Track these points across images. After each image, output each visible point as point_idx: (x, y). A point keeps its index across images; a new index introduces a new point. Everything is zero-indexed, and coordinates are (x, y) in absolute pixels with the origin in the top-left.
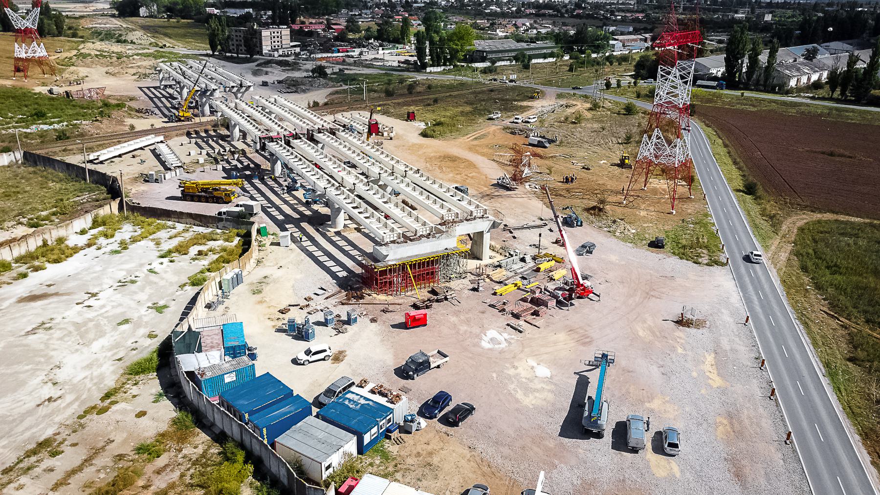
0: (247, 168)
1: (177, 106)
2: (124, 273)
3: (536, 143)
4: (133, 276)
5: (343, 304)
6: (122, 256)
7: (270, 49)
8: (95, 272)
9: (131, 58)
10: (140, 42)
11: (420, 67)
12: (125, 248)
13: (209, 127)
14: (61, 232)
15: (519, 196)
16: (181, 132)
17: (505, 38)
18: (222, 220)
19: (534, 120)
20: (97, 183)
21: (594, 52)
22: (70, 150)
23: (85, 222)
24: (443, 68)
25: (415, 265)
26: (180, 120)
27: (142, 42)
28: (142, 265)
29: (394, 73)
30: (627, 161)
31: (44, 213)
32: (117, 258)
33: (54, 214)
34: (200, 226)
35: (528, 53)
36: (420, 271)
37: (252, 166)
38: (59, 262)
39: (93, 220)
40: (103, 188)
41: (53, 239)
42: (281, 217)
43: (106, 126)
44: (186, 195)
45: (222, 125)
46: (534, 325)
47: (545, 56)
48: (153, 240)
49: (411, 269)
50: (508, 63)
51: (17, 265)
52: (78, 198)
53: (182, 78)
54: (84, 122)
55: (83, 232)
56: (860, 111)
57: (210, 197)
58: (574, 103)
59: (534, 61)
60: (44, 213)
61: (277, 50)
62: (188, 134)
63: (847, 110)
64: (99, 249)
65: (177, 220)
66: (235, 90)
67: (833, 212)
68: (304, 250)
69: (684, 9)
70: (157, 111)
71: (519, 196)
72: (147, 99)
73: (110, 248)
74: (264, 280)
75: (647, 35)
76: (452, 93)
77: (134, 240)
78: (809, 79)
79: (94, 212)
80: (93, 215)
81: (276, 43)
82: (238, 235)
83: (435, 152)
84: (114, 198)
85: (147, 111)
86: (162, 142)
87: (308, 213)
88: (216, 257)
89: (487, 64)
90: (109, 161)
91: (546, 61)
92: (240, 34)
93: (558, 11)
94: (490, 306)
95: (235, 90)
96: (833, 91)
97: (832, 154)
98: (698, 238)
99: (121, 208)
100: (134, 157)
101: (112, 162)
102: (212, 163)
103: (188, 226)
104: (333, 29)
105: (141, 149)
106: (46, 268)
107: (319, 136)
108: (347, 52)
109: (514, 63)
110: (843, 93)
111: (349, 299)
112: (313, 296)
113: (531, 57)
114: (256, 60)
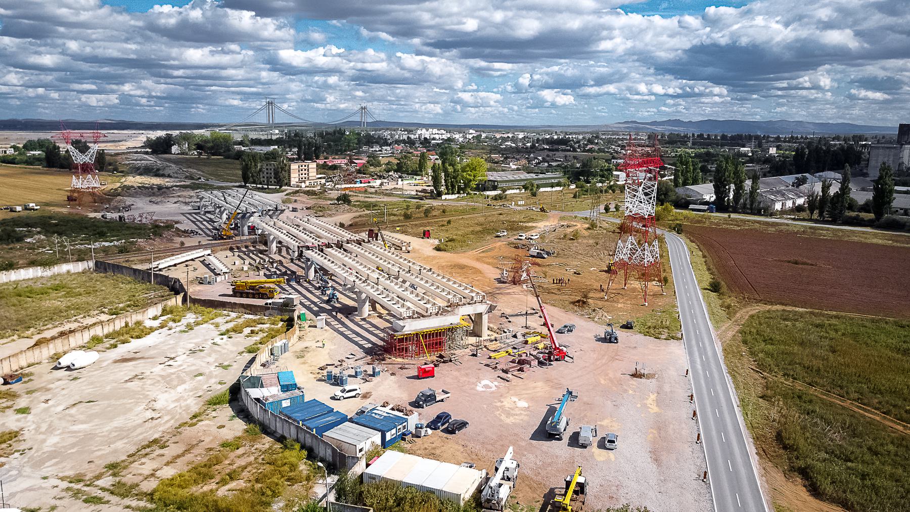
10: (176, 175)
12: (191, 329)
18: (268, 308)
24: (457, 195)
25: (426, 335)
26: (222, 239)
28: (206, 340)
31: (121, 305)
33: (129, 306)
40: (166, 288)
45: (260, 242)
48: (212, 324)
50: (518, 191)
54: (139, 240)
55: (155, 318)
58: (575, 224)
60: (121, 305)
61: (304, 182)
64: (170, 329)
69: (693, 144)
72: (191, 223)
73: (178, 329)
77: (197, 324)
82: (282, 320)
85: (192, 232)
86: (209, 255)
97: (796, 263)
99: (184, 300)
100: (187, 266)
105: (192, 260)
107: (345, 245)
108: (369, 182)
110: (821, 214)
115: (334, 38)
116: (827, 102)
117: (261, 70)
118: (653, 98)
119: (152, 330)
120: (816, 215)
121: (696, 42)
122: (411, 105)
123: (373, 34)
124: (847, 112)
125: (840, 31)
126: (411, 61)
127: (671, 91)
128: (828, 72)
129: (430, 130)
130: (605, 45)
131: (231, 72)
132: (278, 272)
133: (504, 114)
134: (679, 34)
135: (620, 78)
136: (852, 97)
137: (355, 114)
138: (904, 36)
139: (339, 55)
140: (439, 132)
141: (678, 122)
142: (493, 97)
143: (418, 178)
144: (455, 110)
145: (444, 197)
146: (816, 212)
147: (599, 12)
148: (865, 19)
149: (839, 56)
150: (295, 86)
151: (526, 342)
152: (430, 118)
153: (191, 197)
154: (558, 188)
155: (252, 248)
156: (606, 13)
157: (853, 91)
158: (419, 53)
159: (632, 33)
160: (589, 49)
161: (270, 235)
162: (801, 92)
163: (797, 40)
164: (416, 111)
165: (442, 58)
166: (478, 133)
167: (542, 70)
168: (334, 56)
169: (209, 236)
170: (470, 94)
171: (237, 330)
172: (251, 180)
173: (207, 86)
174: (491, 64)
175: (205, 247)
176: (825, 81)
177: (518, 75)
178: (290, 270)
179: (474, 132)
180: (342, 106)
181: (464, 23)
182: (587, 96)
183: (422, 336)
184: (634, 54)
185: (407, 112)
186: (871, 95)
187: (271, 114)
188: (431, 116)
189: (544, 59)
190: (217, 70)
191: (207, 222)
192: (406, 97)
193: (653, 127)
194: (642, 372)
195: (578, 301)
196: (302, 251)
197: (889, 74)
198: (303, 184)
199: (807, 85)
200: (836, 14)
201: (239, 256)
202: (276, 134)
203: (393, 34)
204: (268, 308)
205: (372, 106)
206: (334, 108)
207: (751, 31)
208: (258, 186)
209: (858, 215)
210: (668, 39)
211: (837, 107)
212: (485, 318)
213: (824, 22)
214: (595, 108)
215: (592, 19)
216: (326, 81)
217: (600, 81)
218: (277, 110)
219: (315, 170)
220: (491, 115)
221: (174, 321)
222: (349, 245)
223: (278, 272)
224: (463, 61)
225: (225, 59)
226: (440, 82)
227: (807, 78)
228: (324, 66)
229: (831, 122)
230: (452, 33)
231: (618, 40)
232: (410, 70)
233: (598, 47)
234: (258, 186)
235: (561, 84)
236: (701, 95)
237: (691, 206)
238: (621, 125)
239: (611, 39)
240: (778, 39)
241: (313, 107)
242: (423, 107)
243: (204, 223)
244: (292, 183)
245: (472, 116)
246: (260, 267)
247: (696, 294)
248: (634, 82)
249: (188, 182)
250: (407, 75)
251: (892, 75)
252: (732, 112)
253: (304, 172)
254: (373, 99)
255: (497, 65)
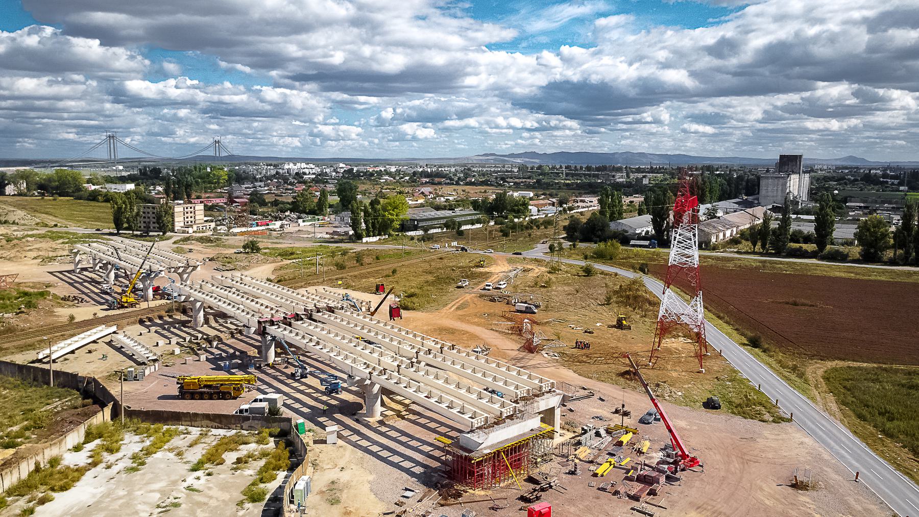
0: (233, 356)
1: (109, 291)
2: (158, 495)
3: (524, 309)
4: (172, 498)
5: (442, 505)
6: (144, 474)
7: (183, 225)
8: (120, 498)
9: (24, 240)
10: (23, 222)
11: (358, 237)
12: (143, 464)
13: (163, 313)
14: (51, 452)
15: (544, 366)
16: (133, 319)
17: (420, 207)
18: (247, 418)
19: (504, 286)
20: (64, 387)
21: (515, 217)
22: (6, 349)
23: (75, 437)
24: (378, 237)
25: (508, 451)
26: (123, 307)
27: (26, 222)
28: (174, 483)
29: (330, 245)
30: (624, 322)
31: (15, 428)
32: (138, 477)
33: (27, 428)
34: (219, 428)
35: (458, 220)
36: (512, 458)
37: (237, 353)
38: (67, 490)
39: (86, 432)
40: (75, 392)
41: (46, 461)
42: (308, 410)
43: (33, 319)
44: (186, 393)
45: (177, 310)
46: (659, 506)
47: (472, 223)
48: (171, 450)
49: (507, 456)
50: (439, 230)
51: (11, 499)
52: (49, 407)
53: (118, 261)
54: (6, 315)
55: (77, 449)
56: (787, 263)
57: (215, 393)
58: (531, 267)
59: (464, 228)
60: (15, 428)
61: (191, 226)
62: (141, 322)
63: (776, 263)
64: (109, 467)
65: (189, 423)
66: (181, 270)
67: (840, 359)
68: (355, 445)
69: (567, 175)
70: (86, 298)
71: (544, 366)
72: (67, 285)
73: (121, 465)
74: (333, 487)
75: (554, 200)
76: (403, 263)
77: (148, 452)
78: (724, 235)
79: (87, 423)
80: (86, 427)
81: (189, 219)
82: (271, 435)
83: (428, 325)
84: (103, 406)
85: (75, 298)
86: (114, 332)
87: (334, 402)
88: (262, 462)
89: (420, 233)
90: (62, 359)
91: (474, 227)
92: (149, 210)
93: (451, 179)
94: (599, 489)
95: (181, 270)
96: (754, 245)
97: (795, 304)
98: (746, 396)
99: (115, 414)
100: (90, 352)
101: (66, 359)
102: (189, 353)
103: (204, 429)
104: (236, 202)
105: (94, 342)
106: (54, 499)
107: (316, 316)
108: (268, 225)
109: (445, 230)
110: (763, 246)
111: (446, 499)
112: (404, 500)
113: (460, 224)
114: (171, 237)
115: (188, 71)
116: (664, 135)
117: (102, 101)
118: (511, 131)
119: (80, 471)
120: (758, 247)
121: (551, 78)
122: (268, 138)
123: (230, 65)
124: (681, 144)
125: (676, 71)
126: (272, 94)
127: (528, 125)
128: (667, 108)
129: (298, 165)
130: (469, 81)
131: (71, 103)
132: (224, 355)
133: (365, 147)
134: (539, 71)
135: (479, 111)
136: (685, 131)
137: (207, 148)
138: (730, 76)
139: (194, 87)
140: (308, 167)
141: (533, 155)
142: (354, 131)
143: (321, 217)
144: (314, 143)
145: (365, 240)
146: (759, 244)
147: (466, 50)
148: (696, 60)
149: (679, 94)
150: (142, 119)
151: (620, 444)
152: (288, 152)
153: (55, 250)
154: (478, 226)
155: (167, 319)
156: (473, 51)
157: (686, 126)
158: (277, 85)
159: (494, 69)
160: (454, 85)
161: (196, 301)
162: (643, 126)
163: (640, 79)
164: (274, 145)
165: (302, 90)
166: (349, 167)
167: (404, 104)
168: (189, 87)
169: (101, 304)
170: (331, 127)
171: (213, 458)
172: (125, 225)
173: (38, 118)
174: (355, 98)
175: (105, 321)
176: (665, 116)
177: (379, 108)
178: (239, 350)
179: (344, 166)
180: (192, 140)
181: (332, 56)
182: (447, 129)
183: (504, 452)
184: (496, 90)
185: (264, 145)
186: (701, 128)
187: (112, 149)
188: (290, 150)
189: (409, 93)
190: (52, 101)
191: (89, 283)
192: (264, 130)
193: (512, 159)
194: (805, 480)
195: (627, 373)
196: (265, 328)
197: (716, 110)
198: (190, 229)
199: (649, 119)
200: (672, 55)
201: (156, 332)
202: (120, 170)
203: (252, 66)
204: (247, 418)
205: (227, 140)
206: (183, 142)
207: (601, 69)
208: (135, 233)
209: (801, 247)
210: (530, 75)
211: (674, 140)
212: (558, 412)
213: (661, 63)
214: (456, 141)
215: (459, 56)
216: (175, 115)
217: (463, 114)
218: (119, 144)
219: (202, 212)
220: (352, 148)
221: (111, 451)
222: (320, 314)
223: (224, 355)
224: (324, 94)
225: (66, 89)
226: (303, 115)
227: (649, 113)
228: (178, 98)
229: (669, 153)
230: (317, 65)
231: (483, 76)
232: (271, 103)
233: (463, 82)
234: (135, 233)
235: (425, 118)
236: (556, 128)
237: (632, 242)
238: (481, 158)
239: (477, 74)
240: (624, 77)
241: (161, 142)
242: (282, 140)
243: (86, 284)
244: (176, 228)
245: (331, 150)
246: (195, 347)
247: (739, 350)
248: (494, 116)
249: (43, 231)
250: (268, 107)
251: (719, 111)
252: (582, 144)
253: (189, 215)
254: (227, 132)
255: (362, 99)
